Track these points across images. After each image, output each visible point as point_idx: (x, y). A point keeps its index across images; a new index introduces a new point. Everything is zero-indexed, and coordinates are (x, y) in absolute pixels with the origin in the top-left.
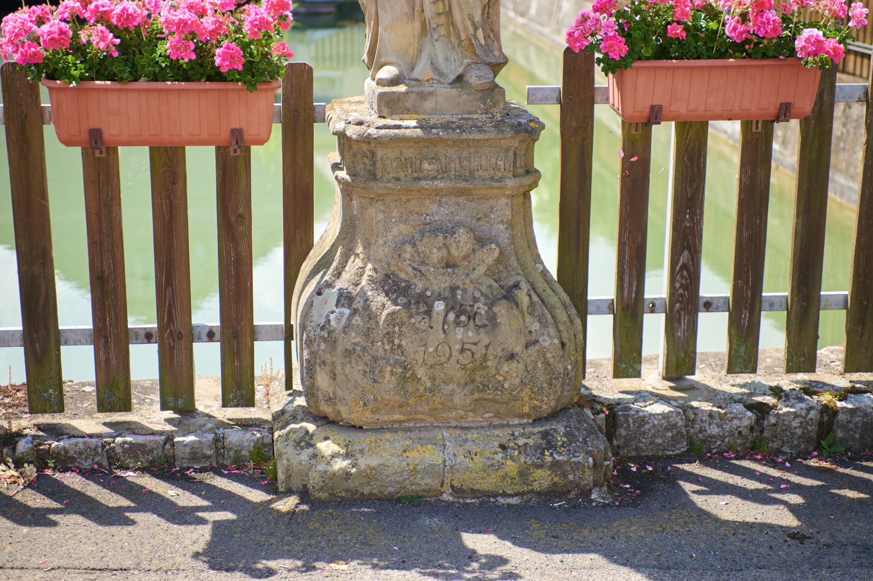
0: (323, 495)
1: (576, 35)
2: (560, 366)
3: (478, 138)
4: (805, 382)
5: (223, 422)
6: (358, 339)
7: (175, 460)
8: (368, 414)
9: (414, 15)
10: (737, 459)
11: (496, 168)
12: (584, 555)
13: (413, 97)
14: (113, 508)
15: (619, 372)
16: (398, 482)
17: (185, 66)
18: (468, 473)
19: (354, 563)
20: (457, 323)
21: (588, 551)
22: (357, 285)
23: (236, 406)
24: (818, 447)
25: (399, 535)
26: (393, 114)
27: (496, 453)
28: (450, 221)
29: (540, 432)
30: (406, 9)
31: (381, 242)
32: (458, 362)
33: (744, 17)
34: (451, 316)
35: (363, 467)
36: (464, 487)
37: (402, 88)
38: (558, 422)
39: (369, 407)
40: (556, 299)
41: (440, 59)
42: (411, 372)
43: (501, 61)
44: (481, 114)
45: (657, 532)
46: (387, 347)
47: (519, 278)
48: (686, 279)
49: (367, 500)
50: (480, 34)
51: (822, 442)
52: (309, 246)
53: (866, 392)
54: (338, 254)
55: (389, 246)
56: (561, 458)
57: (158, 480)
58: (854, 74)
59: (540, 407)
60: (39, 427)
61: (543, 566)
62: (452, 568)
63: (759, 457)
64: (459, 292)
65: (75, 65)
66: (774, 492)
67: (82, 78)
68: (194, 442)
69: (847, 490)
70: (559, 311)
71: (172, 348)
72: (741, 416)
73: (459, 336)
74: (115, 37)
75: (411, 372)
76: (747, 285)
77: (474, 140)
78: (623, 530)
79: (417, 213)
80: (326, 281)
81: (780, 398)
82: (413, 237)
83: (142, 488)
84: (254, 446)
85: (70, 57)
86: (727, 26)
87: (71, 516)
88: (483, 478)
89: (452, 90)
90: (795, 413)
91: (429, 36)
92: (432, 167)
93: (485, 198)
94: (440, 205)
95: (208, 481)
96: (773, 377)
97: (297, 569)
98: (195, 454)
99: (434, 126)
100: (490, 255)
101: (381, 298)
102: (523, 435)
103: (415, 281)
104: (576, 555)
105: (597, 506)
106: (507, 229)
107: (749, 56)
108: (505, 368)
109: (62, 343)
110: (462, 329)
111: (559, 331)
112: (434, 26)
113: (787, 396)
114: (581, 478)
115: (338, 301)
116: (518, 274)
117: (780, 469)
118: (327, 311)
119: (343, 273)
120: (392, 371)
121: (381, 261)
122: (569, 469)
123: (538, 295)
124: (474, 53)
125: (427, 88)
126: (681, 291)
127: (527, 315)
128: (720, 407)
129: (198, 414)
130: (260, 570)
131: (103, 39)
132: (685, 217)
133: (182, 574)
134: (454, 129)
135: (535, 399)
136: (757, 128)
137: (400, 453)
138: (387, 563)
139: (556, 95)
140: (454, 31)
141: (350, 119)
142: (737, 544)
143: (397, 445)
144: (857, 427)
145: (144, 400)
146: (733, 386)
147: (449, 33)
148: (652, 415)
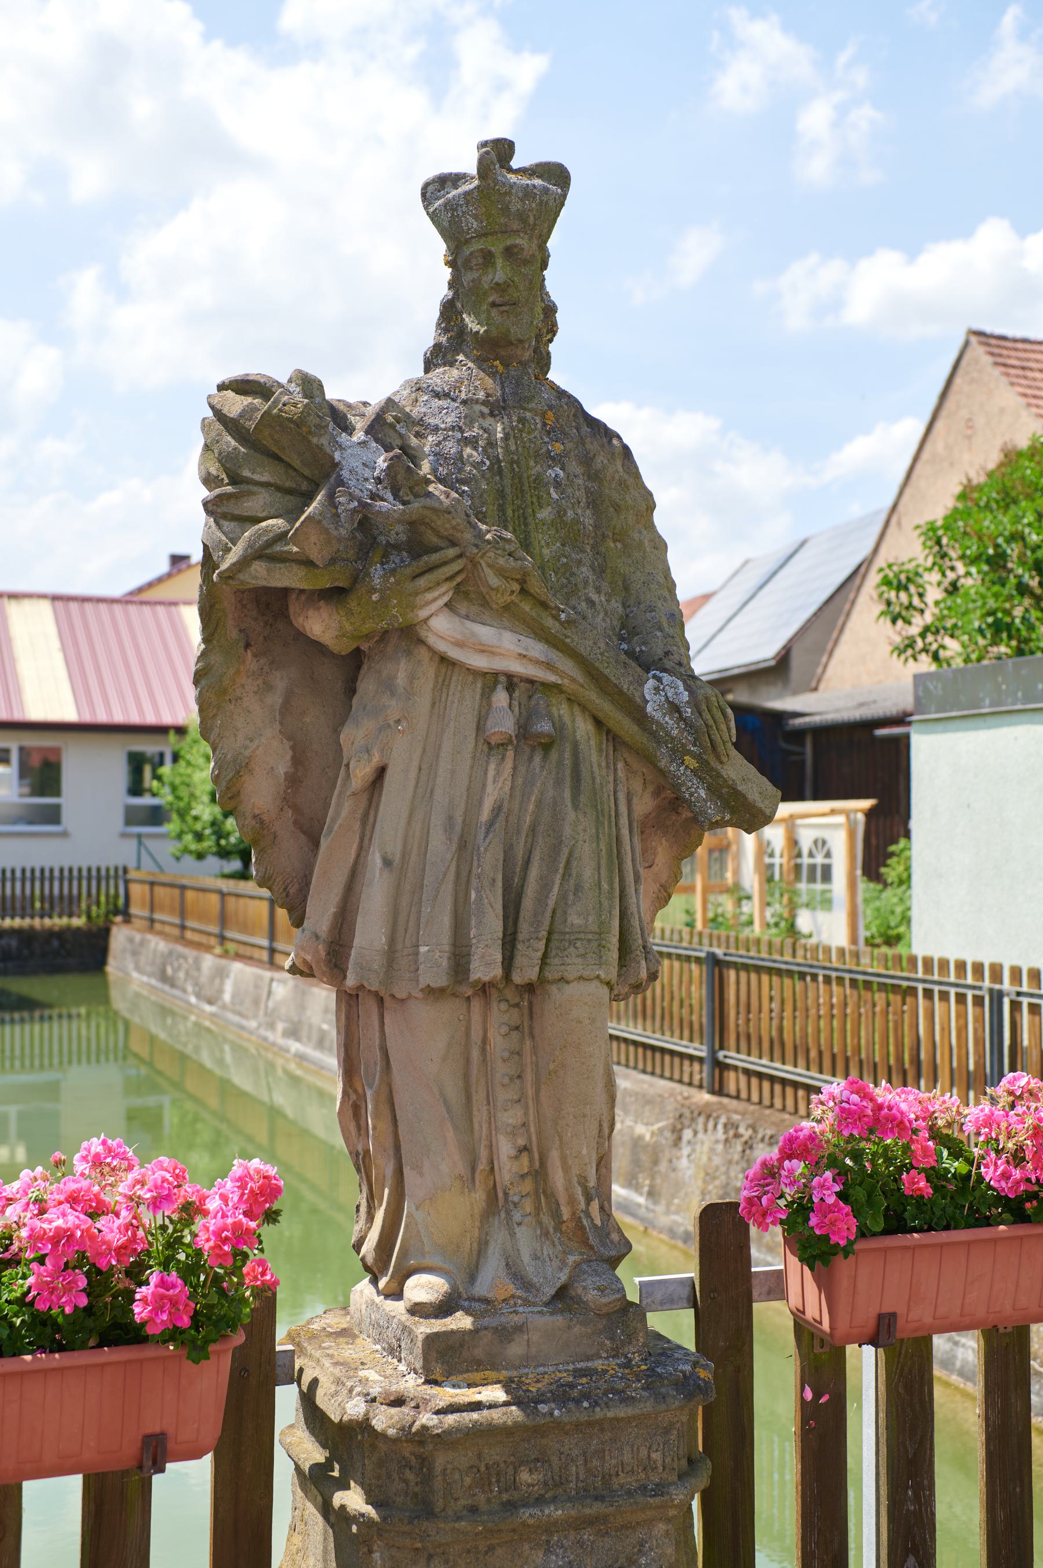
3: (622, 1415)
9: (473, 1179)
11: (648, 1466)
13: (487, 1336)
26: (451, 1375)
30: (462, 1169)
37: (461, 1321)
41: (526, 1258)
44: (607, 1358)
58: (737, 1097)
89: (554, 1318)
91: (503, 1215)
92: (536, 1477)
94: (548, 1551)
124: (585, 1243)
132: (906, 1493)
134: (578, 1402)
139: (686, 1292)
147: (538, 1208)
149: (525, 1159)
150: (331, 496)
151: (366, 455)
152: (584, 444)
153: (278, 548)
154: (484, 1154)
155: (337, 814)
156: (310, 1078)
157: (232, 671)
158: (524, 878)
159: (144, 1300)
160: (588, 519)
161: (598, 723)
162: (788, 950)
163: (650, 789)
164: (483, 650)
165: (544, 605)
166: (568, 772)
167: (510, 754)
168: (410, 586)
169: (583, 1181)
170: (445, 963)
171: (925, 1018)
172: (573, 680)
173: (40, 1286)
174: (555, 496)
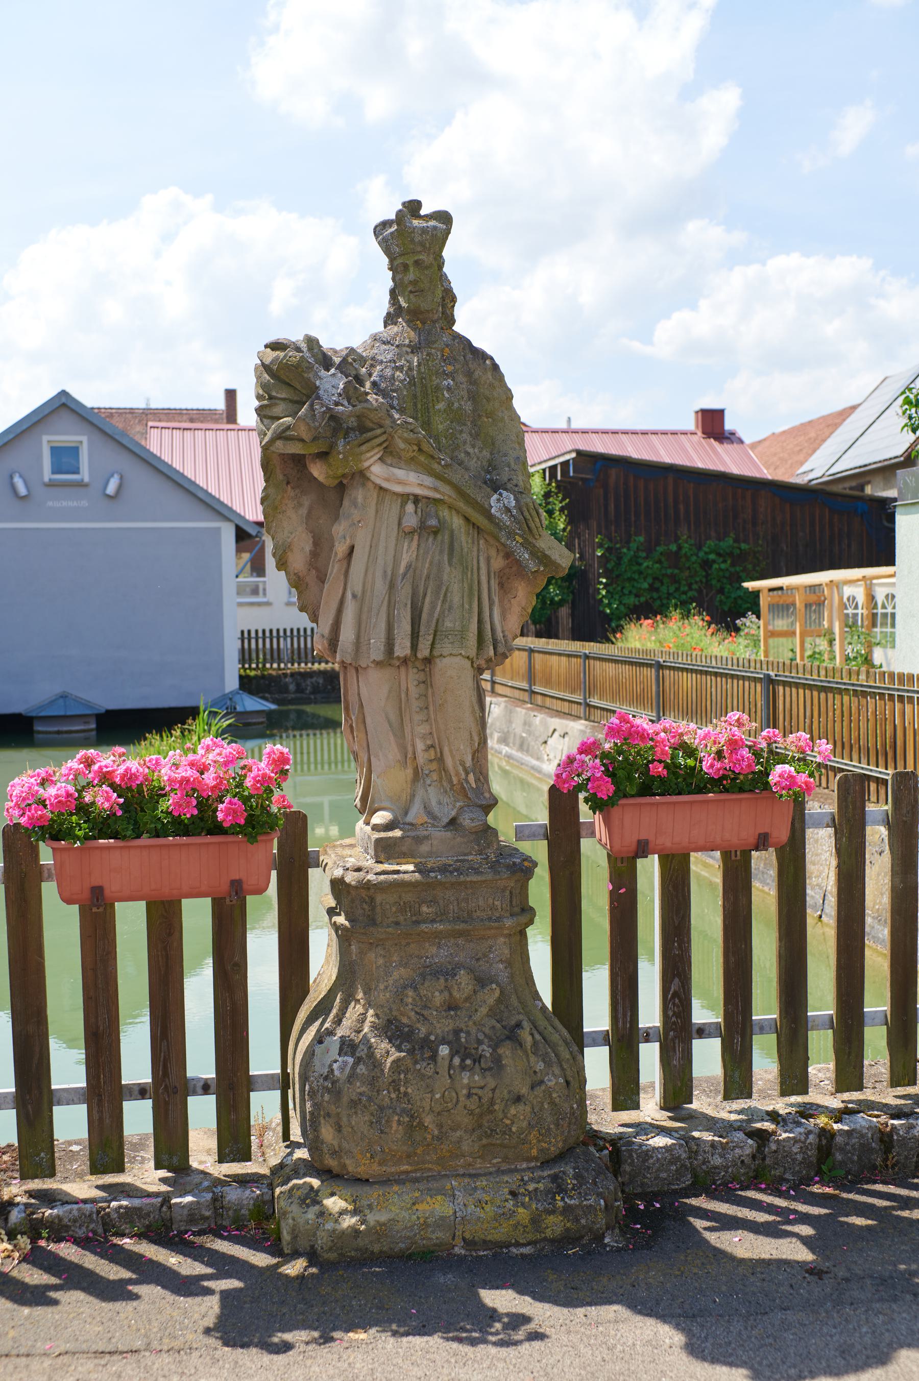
0: (332, 1256)
1: (564, 776)
2: (566, 1105)
4: (799, 1105)
5: (219, 1179)
6: (363, 1089)
7: (172, 1224)
8: (375, 1167)
10: (742, 1190)
11: (493, 908)
12: (607, 1307)
14: (114, 1281)
15: (617, 1106)
16: (409, 1238)
17: (186, 821)
18: (479, 1224)
19: (373, 1331)
20: (463, 1067)
21: (610, 1302)
22: (359, 1032)
23: (232, 1161)
24: (819, 1172)
25: (416, 1296)
27: (507, 1200)
28: (450, 963)
29: (549, 1176)
30: (399, 757)
31: (382, 987)
32: (465, 1107)
33: (719, 754)
34: (457, 1061)
35: (372, 1223)
36: (476, 1238)
37: (397, 833)
38: (566, 1164)
39: (376, 1159)
40: (557, 1036)
41: (434, 803)
42: (417, 1120)
43: (493, 802)
45: (676, 1276)
46: (393, 1096)
47: (521, 1017)
48: (678, 1007)
49: (377, 1259)
50: (471, 777)
51: (823, 1167)
52: (304, 990)
53: (859, 1112)
54: (338, 1000)
55: (390, 991)
56: (572, 1202)
57: (156, 1247)
59: (548, 1149)
60: (31, 1194)
61: (567, 1322)
62: (475, 1331)
63: (763, 1186)
64: (463, 1035)
65: (79, 825)
66: (784, 1223)
67: (86, 838)
68: (191, 1203)
69: (854, 1217)
70: (562, 1049)
71: (167, 1103)
72: (742, 1144)
73: (466, 1081)
74: (119, 796)
75: (417, 1120)
76: (737, 1009)
77: (471, 882)
78: (641, 1277)
79: (418, 957)
80: (327, 1029)
81: (778, 1124)
82: (414, 980)
83: (141, 1256)
84: (254, 1204)
85: (74, 818)
86: (704, 763)
87: (72, 1292)
88: (495, 1228)
90: (794, 1138)
93: (483, 938)
94: (439, 947)
95: (208, 1245)
96: (767, 1101)
97: (314, 1341)
98: (193, 1215)
99: (432, 870)
100: (491, 996)
101: (384, 1045)
102: (532, 1180)
103: (418, 1025)
104: (599, 1307)
105: (611, 1250)
106: (506, 968)
107: (726, 790)
108: (513, 1111)
109: (55, 1103)
110: (468, 1073)
111: (563, 1069)
112: (427, 772)
113: (784, 1120)
114: (593, 1222)
115: (341, 1049)
116: (519, 1013)
117: (785, 1198)
118: (330, 1060)
119: (344, 1019)
120: (399, 1120)
121: (382, 1006)
122: (581, 1213)
123: (540, 1034)
124: (466, 796)
125: (422, 833)
126: (674, 1019)
127: (531, 1055)
128: (720, 1137)
129: (193, 1171)
130: (276, 1344)
131: (108, 799)
133: (196, 1354)
134: (452, 872)
135: (543, 1141)
136: (736, 856)
137: (409, 1206)
138: (406, 1328)
139: (542, 831)
140: (446, 775)
141: (348, 865)
142: (758, 1284)
143: (406, 1197)
144: (854, 1149)
145: (134, 1157)
146: (730, 1112)
147: (441, 778)
148: (655, 1149)
149: (432, 751)
150: (312, 405)
151: (334, 381)
152: (467, 365)
153: (288, 433)
154: (410, 749)
155: (332, 571)
156: (515, 772)
157: (279, 497)
158: (423, 603)
159: (221, 810)
160: (468, 407)
161: (467, 519)
162: (815, 672)
163: (502, 554)
164: (400, 482)
165: (432, 457)
166: (446, 546)
167: (416, 537)
168: (357, 450)
169: (462, 763)
170: (382, 648)
171: (899, 716)
172: (450, 497)
173: (174, 804)
174: (447, 395)
